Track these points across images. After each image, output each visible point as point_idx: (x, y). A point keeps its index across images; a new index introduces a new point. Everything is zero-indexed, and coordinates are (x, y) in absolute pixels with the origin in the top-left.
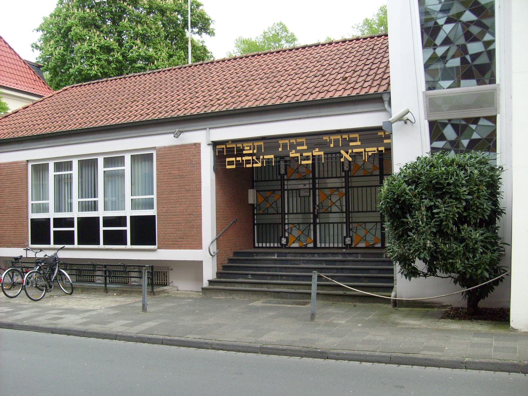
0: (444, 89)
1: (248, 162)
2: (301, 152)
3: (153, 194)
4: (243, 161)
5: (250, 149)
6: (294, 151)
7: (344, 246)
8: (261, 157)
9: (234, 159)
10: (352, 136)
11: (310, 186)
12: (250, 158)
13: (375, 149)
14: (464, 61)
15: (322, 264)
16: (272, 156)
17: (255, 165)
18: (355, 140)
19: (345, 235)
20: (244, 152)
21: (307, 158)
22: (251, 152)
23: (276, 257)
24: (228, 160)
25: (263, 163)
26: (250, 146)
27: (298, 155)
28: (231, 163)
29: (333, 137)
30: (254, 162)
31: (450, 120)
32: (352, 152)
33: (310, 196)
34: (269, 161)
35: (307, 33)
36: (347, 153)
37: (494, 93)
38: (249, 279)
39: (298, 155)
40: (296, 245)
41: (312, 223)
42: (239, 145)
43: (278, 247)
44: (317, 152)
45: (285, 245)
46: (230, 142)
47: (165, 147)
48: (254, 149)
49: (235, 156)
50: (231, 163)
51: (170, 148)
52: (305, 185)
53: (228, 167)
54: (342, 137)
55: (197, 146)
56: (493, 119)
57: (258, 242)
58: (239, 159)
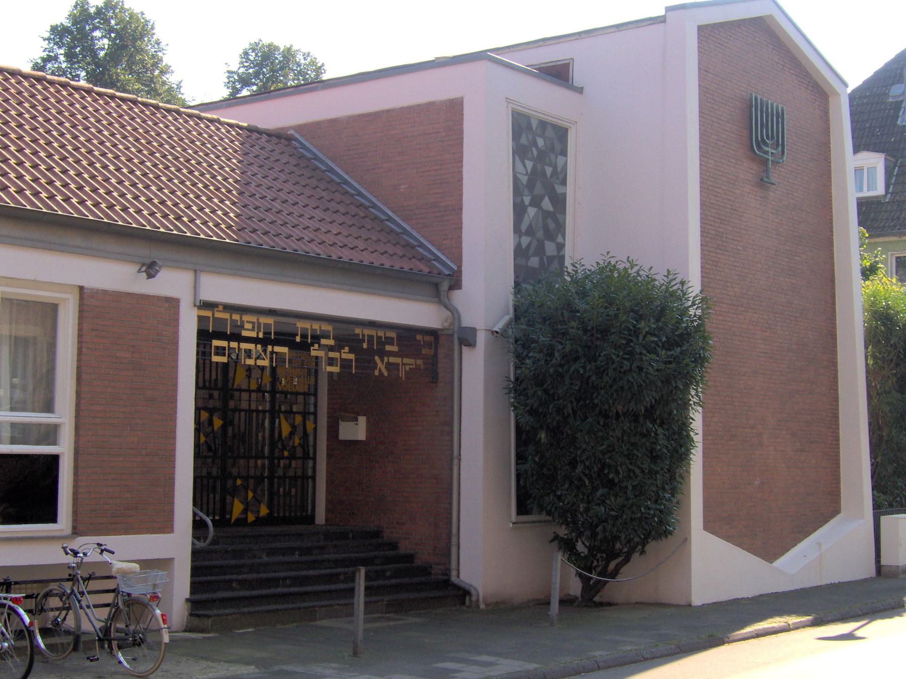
1: (248, 353)
3: (48, 407)
5: (253, 330)
6: (316, 346)
9: (224, 343)
12: (251, 346)
13: (412, 361)
14: (541, 260)
15: (277, 586)
17: (260, 363)
18: (389, 341)
20: (245, 333)
25: (271, 359)
26: (253, 323)
28: (220, 351)
29: (367, 332)
35: (339, 58)
36: (382, 361)
37: (568, 64)
42: (236, 317)
46: (221, 308)
47: (105, 292)
50: (220, 351)
51: (117, 296)
53: (215, 359)
54: (326, 354)
55: (173, 303)
58: (234, 345)
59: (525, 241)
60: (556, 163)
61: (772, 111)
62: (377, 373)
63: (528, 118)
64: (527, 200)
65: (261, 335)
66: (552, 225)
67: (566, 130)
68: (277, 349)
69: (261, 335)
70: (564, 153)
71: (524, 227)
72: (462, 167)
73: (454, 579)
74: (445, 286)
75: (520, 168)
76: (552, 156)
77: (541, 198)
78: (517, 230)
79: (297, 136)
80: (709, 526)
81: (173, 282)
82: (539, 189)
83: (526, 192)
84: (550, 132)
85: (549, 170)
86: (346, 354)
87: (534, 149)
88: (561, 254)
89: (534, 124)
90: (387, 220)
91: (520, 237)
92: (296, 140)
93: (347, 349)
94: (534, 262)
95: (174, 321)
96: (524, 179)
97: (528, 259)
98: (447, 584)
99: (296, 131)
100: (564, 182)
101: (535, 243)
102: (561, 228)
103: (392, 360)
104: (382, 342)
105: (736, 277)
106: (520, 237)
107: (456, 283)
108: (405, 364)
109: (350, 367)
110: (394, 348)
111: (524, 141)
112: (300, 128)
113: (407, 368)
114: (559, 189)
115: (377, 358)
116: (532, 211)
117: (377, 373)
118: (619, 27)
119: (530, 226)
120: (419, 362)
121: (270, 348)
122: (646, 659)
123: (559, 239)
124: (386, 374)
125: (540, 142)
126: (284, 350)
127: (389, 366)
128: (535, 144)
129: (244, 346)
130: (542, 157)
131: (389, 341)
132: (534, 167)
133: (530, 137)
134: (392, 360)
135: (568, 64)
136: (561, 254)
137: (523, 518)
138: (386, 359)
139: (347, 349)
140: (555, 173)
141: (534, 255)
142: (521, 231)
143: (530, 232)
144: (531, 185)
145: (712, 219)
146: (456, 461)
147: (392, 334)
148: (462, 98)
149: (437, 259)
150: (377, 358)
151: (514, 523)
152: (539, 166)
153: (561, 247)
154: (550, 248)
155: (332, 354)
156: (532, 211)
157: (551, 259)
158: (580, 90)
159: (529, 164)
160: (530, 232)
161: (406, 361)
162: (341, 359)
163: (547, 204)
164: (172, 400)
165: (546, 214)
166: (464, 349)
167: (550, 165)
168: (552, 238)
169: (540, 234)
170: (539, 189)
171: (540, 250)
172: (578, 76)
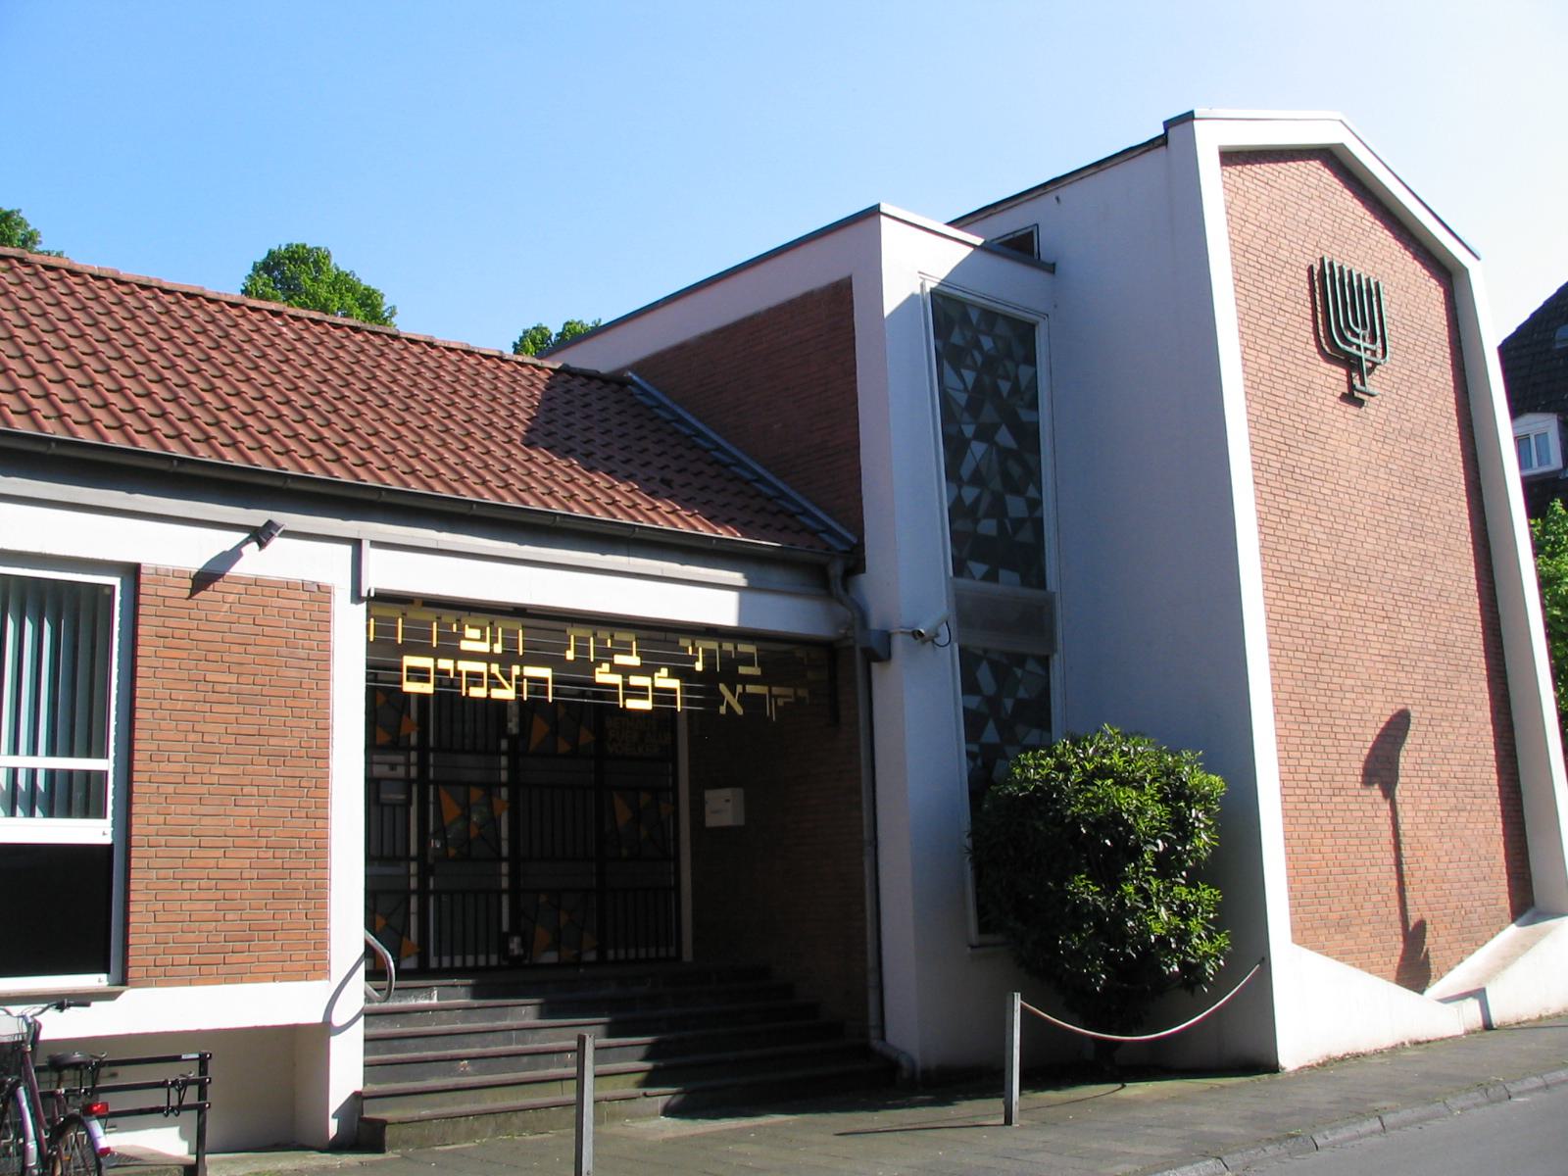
0: (973, 578)
1: (475, 679)
2: (626, 671)
4: (458, 673)
5: (483, 639)
6: (606, 667)
7: (505, 963)
8: (516, 670)
9: (427, 662)
10: (622, 636)
11: (408, 772)
12: (480, 667)
13: (789, 691)
14: (1001, 527)
16: (545, 673)
17: (496, 694)
18: (748, 660)
19: (505, 927)
20: (465, 645)
21: (639, 692)
22: (484, 647)
23: (435, 1001)
24: (409, 661)
25: (519, 690)
27: (617, 679)
28: (419, 675)
29: (703, 645)
30: (494, 682)
31: (986, 651)
32: (522, 673)
33: (409, 802)
34: (538, 683)
37: (1032, 233)
38: (464, 1074)
39: (617, 679)
40: (551, 957)
41: (504, 891)
43: (498, 968)
44: (664, 680)
45: (519, 958)
48: (494, 640)
49: (436, 654)
50: (419, 675)
52: (393, 766)
53: (409, 687)
56: (1044, 662)
57: (439, 955)
58: (446, 664)
59: (969, 494)
60: (1017, 377)
61: (1360, 286)
62: (723, 710)
63: (962, 305)
64: (969, 430)
65: (498, 648)
66: (1016, 470)
67: (1031, 328)
68: (531, 671)
69: (498, 648)
70: (1031, 360)
71: (966, 471)
72: (855, 381)
73: (876, 1043)
74: (836, 569)
75: (952, 379)
76: (1010, 365)
77: (996, 427)
78: (952, 474)
79: (635, 378)
80: (1302, 935)
81: (304, 557)
82: (989, 414)
83: (966, 417)
84: (1001, 329)
85: (1005, 387)
86: (664, 680)
87: (977, 354)
88: (1037, 514)
89: (974, 316)
90: (756, 481)
91: (960, 488)
92: (633, 383)
93: (664, 672)
94: (988, 527)
95: (322, 623)
96: (962, 398)
97: (976, 521)
98: (865, 1051)
99: (635, 373)
100: (1034, 405)
101: (986, 500)
102: (1033, 475)
103: (750, 689)
104: (731, 663)
105: (1324, 537)
106: (960, 488)
107: (855, 561)
108: (777, 697)
109: (674, 701)
110: (755, 671)
111: (956, 338)
112: (639, 367)
113: (781, 702)
114: (1025, 416)
115: (722, 687)
116: (978, 449)
117: (723, 710)
118: (1099, 165)
119: (977, 471)
120: (802, 692)
121: (516, 670)
122: (646, 1116)
123: (1032, 492)
124: (739, 710)
125: (987, 343)
126: (545, 673)
127: (744, 699)
128: (978, 346)
129: (465, 666)
130: (990, 364)
131: (748, 660)
132: (978, 381)
133: (969, 334)
134: (750, 689)
135: (1032, 233)
136: (1037, 514)
137: (989, 938)
138: (739, 688)
139: (664, 672)
140: (1015, 390)
141: (987, 516)
142: (960, 478)
143: (977, 479)
144: (974, 406)
145: (1273, 444)
146: (868, 849)
147: (746, 648)
148: (850, 278)
149: (829, 530)
150: (722, 687)
151: (972, 947)
152: (987, 380)
153: (1035, 504)
154: (1016, 506)
155: (636, 681)
156: (978, 449)
157: (1019, 523)
158: (1051, 268)
159: (969, 376)
160: (977, 479)
161: (776, 690)
162: (655, 689)
163: (1004, 437)
164: (319, 754)
165: (1004, 453)
166: (875, 666)
167: (1006, 378)
168: (1018, 491)
169: (996, 484)
170: (989, 414)
171: (998, 509)
172: (1047, 244)
